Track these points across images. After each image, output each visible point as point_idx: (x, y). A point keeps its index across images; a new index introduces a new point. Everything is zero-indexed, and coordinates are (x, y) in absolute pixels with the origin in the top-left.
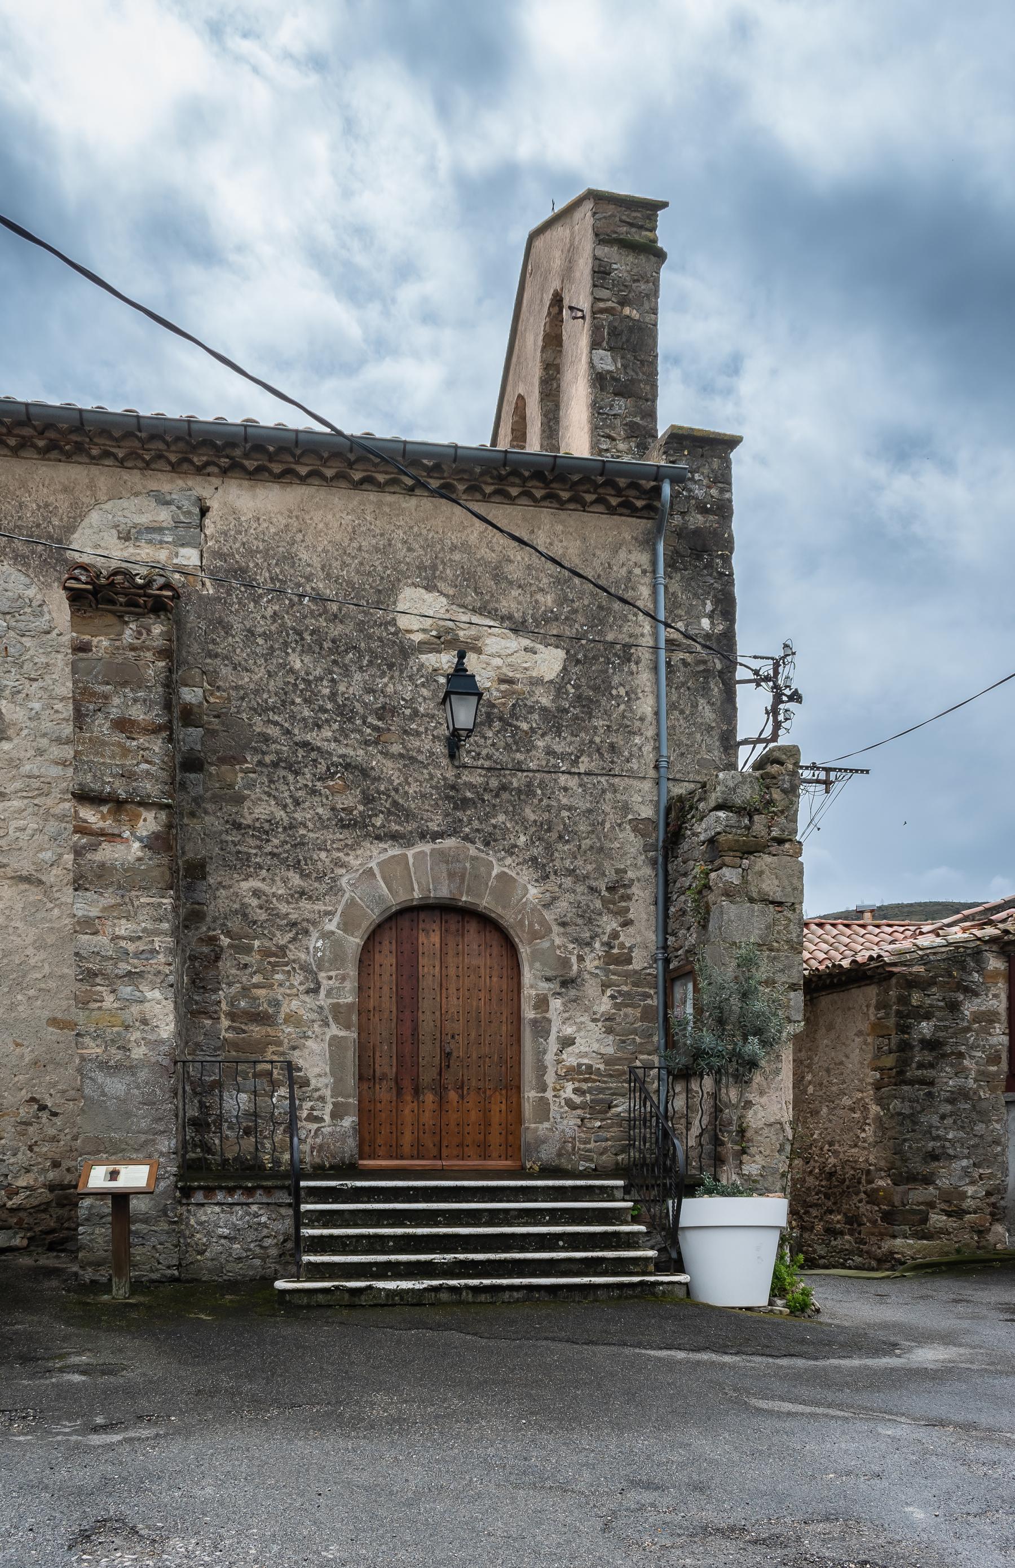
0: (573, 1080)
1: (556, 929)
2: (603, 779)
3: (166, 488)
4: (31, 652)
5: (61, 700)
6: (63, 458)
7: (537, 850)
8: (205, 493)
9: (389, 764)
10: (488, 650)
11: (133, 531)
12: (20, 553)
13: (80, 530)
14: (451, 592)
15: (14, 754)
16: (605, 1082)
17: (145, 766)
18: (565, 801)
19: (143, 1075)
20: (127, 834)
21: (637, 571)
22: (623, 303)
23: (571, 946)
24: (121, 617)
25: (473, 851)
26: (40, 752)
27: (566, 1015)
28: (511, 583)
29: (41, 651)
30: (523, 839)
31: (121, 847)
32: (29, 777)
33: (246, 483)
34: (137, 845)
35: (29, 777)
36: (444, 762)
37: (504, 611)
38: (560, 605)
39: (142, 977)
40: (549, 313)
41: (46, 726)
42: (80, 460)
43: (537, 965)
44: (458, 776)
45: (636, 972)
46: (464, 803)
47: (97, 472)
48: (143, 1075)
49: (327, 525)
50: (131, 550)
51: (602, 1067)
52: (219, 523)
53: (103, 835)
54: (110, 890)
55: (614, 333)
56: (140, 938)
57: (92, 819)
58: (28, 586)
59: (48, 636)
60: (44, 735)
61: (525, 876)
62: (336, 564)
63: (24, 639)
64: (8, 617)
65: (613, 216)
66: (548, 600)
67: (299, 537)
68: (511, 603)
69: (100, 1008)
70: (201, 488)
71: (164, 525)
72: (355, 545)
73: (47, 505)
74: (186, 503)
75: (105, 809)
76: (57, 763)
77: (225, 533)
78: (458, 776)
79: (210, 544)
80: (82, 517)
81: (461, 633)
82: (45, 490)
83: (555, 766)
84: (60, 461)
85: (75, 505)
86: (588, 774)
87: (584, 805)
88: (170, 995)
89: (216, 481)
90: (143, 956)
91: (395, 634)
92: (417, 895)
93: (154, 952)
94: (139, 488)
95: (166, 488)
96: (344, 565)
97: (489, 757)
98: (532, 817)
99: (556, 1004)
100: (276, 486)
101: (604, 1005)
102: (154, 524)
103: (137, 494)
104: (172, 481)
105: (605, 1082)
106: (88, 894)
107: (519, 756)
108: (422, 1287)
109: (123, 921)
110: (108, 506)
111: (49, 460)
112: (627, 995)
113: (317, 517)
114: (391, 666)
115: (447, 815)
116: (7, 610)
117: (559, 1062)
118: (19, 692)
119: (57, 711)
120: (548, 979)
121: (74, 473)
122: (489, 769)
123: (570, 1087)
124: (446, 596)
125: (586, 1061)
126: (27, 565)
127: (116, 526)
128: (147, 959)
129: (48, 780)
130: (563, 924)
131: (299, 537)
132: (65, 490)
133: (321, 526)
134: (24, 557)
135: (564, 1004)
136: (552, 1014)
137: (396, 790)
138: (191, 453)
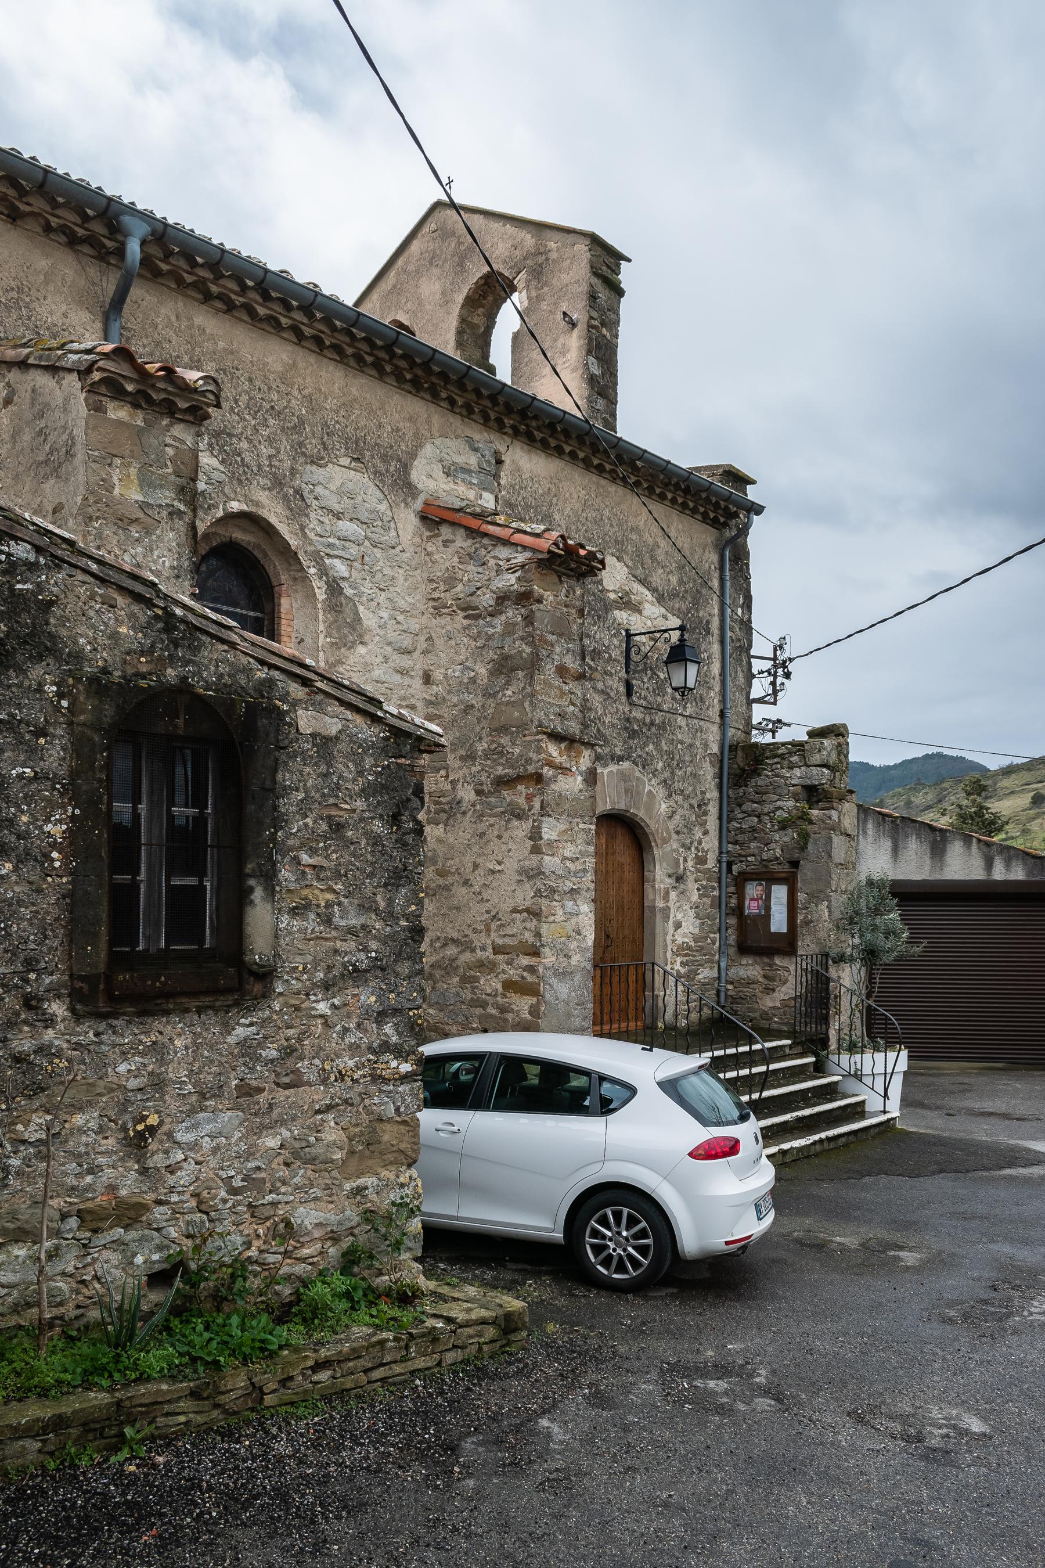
0: (680, 955)
1: (674, 836)
2: (696, 721)
3: (477, 437)
4: (381, 563)
5: (402, 613)
6: (414, 392)
7: (666, 775)
8: (502, 449)
9: (597, 698)
10: (646, 613)
11: (452, 468)
12: (378, 469)
13: (418, 459)
14: (630, 564)
15: (368, 659)
16: (694, 956)
17: (572, 708)
18: (680, 737)
19: (578, 978)
20: (574, 769)
21: (713, 567)
22: (603, 324)
23: (681, 850)
24: (560, 577)
25: (637, 774)
26: (386, 660)
27: (678, 904)
28: (658, 563)
29: (388, 564)
30: (660, 764)
31: (571, 780)
32: (377, 682)
33: (526, 447)
34: (579, 778)
35: (377, 682)
36: (624, 699)
37: (654, 585)
38: (680, 585)
39: (579, 893)
40: (477, 282)
41: (392, 635)
42: (425, 396)
43: (664, 865)
44: (630, 711)
45: (709, 870)
46: (633, 734)
47: (433, 410)
48: (578, 978)
49: (571, 494)
50: (452, 485)
51: (692, 944)
52: (510, 477)
53: (561, 768)
54: (564, 817)
55: (599, 347)
56: (577, 858)
57: (555, 754)
58: (380, 501)
59: (393, 551)
60: (390, 644)
61: (661, 793)
62: (574, 528)
63: (376, 550)
64: (365, 526)
65: (599, 256)
66: (674, 579)
67: (555, 500)
68: (657, 579)
69: (554, 921)
70: (500, 444)
71: (472, 468)
72: (584, 515)
73: (398, 430)
74: (487, 453)
75: (563, 746)
76: (397, 671)
77: (513, 486)
78: (630, 711)
79: (503, 493)
80: (421, 446)
81: (633, 597)
82: (397, 416)
83: (676, 709)
84: (410, 392)
85: (417, 435)
86: (690, 717)
87: (688, 741)
88: (593, 909)
89: (508, 440)
90: (579, 875)
91: (601, 591)
92: (609, 807)
93: (585, 871)
94: (459, 431)
95: (477, 437)
96: (578, 530)
97: (645, 698)
98: (665, 748)
99: (673, 895)
100: (543, 455)
101: (695, 898)
102: (466, 466)
103: (457, 437)
104: (481, 433)
105: (694, 956)
106: (551, 819)
107: (659, 699)
108: (808, 1142)
109: (569, 844)
110: (438, 442)
111: (403, 389)
112: (704, 887)
113: (566, 487)
114: (599, 617)
115: (625, 742)
116: (366, 520)
117: (673, 941)
118: (372, 600)
119: (398, 623)
120: (670, 876)
121: (417, 407)
122: (646, 708)
123: (679, 960)
124: (627, 566)
125: (686, 940)
126: (382, 481)
127: (441, 461)
128: (581, 877)
129: (391, 686)
130: (678, 833)
131: (555, 499)
132: (411, 419)
133: (567, 495)
134: (381, 474)
135: (678, 896)
136: (671, 904)
137: (599, 719)
138: (505, 415)
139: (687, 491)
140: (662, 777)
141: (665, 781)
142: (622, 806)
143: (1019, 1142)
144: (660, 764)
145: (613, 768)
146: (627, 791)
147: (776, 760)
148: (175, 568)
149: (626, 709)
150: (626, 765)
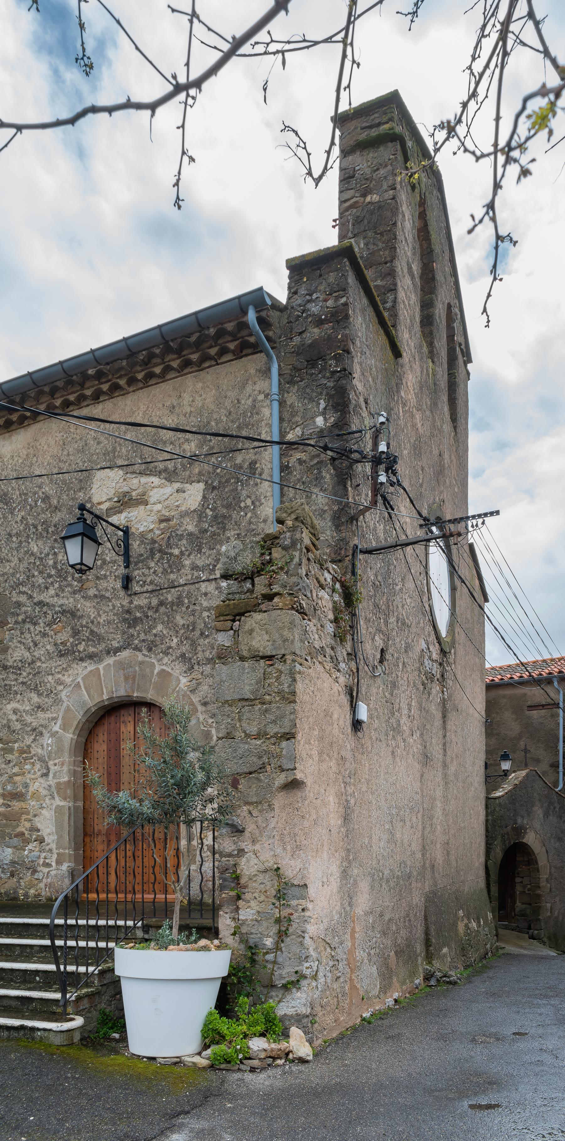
1: (200, 708)
9: (88, 604)
25: (141, 658)
30: (175, 640)
61: (177, 670)
72: (65, 453)
78: (131, 602)
92: (105, 697)
100: (23, 430)
115: (124, 633)
130: (205, 704)
139: (168, 349)
140: (178, 653)
141: (183, 655)
142: (122, 692)
143: (274, 356)
144: (175, 640)
145: (110, 660)
146: (126, 678)
147: (390, 604)
148: (105, 1014)
149: (125, 602)
150: (125, 654)
